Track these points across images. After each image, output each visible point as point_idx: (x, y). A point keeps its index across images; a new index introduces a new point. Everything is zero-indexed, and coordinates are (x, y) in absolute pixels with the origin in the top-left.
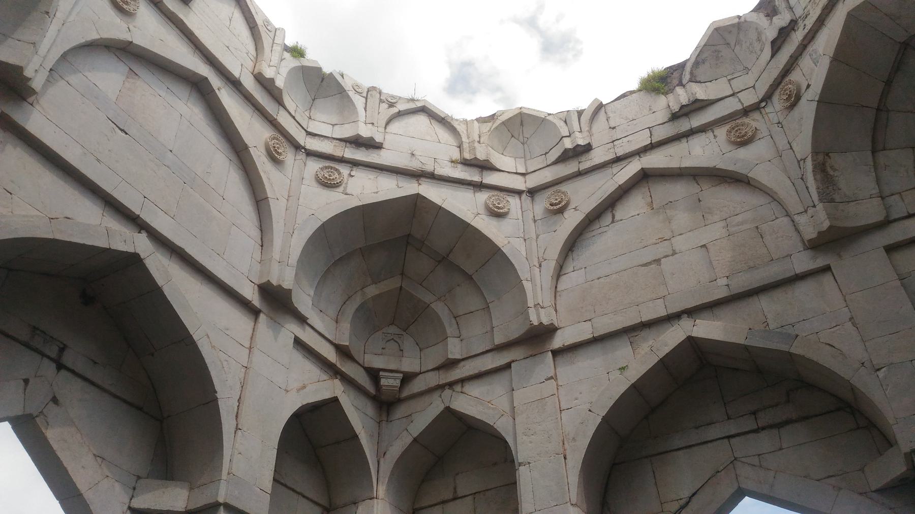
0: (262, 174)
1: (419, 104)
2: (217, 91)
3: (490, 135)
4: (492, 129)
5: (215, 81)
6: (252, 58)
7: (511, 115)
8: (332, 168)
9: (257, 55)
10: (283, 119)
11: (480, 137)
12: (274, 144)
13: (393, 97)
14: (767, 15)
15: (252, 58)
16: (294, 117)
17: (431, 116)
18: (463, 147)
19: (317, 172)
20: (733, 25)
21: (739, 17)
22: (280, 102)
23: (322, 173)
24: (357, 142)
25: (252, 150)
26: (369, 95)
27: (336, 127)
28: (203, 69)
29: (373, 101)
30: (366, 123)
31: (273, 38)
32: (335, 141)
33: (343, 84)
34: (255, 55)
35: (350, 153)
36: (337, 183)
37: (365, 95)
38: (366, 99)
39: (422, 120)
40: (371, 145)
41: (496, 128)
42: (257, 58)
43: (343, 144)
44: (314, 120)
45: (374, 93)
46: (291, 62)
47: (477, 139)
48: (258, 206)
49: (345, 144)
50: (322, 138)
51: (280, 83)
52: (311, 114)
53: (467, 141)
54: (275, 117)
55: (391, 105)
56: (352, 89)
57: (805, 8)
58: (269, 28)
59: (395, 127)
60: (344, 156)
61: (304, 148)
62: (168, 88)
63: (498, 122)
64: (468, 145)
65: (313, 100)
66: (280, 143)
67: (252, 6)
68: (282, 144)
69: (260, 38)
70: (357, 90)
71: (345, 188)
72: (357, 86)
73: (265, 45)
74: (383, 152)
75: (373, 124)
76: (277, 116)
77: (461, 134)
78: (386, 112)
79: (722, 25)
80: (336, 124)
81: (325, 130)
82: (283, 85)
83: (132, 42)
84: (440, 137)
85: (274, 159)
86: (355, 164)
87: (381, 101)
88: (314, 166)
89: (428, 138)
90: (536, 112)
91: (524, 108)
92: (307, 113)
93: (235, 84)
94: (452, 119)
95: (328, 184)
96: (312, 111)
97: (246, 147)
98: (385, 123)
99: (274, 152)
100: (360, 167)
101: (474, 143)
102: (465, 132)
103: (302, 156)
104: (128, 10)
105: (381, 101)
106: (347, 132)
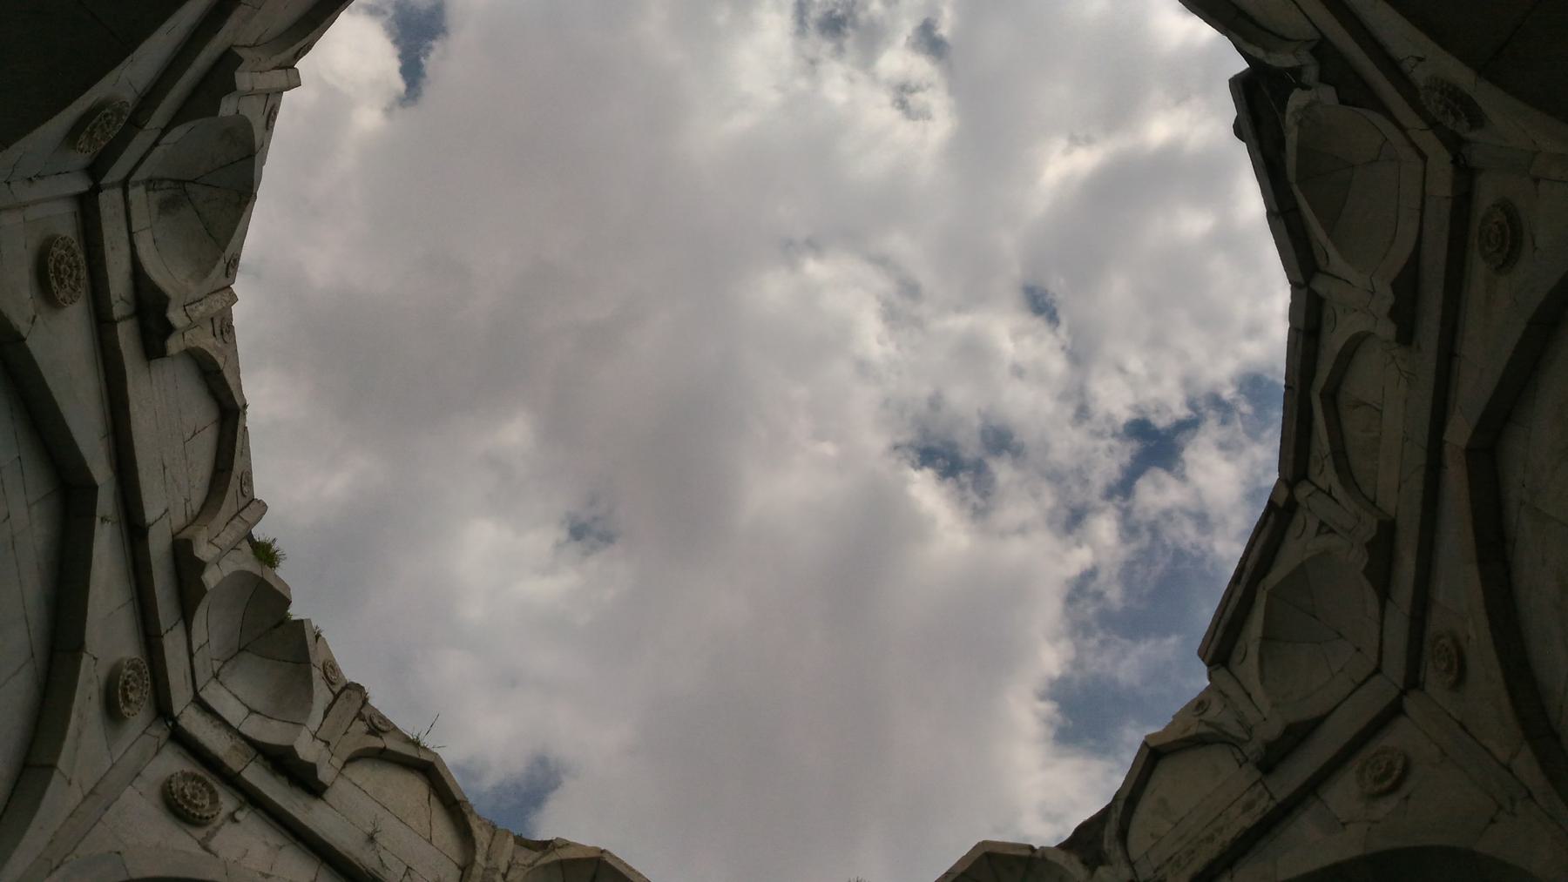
0: (74, 716)
1: (424, 756)
2: (98, 520)
3: (528, 874)
4: (539, 863)
5: (106, 502)
6: (189, 513)
7: (581, 855)
8: (205, 783)
9: (199, 513)
10: (173, 646)
11: (509, 868)
12: (129, 676)
13: (383, 719)
14: (1084, 862)
15: (189, 513)
16: (191, 655)
17: (435, 788)
18: (471, 870)
19: (172, 776)
20: (1018, 858)
21: (1031, 848)
22: (186, 614)
23: (182, 784)
24: (282, 762)
25: (86, 660)
26: (343, 695)
27: (254, 717)
28: (101, 471)
29: (347, 707)
30: (314, 737)
31: (241, 506)
32: (238, 739)
33: (311, 649)
34: (196, 513)
35: (256, 776)
36: (200, 817)
37: (337, 689)
38: (336, 697)
39: (414, 789)
40: (306, 780)
41: (546, 866)
42: (196, 518)
43: (252, 752)
44: (221, 683)
45: (355, 695)
46: (244, 561)
47: (503, 869)
48: (12, 794)
49: (254, 754)
50: (218, 722)
51: (211, 578)
52: (223, 671)
53: (484, 864)
54: (163, 631)
55: (374, 731)
56: (321, 667)
57: (1158, 868)
58: (245, 489)
59: (364, 774)
60: (242, 773)
61: (175, 720)
62: (19, 457)
63: (553, 857)
64: (481, 872)
65: (240, 650)
66: (140, 681)
67: (241, 437)
68: (142, 685)
69: (224, 493)
70: (329, 674)
71: (210, 836)
72: (332, 668)
73: (225, 507)
74: (318, 806)
75: (328, 744)
76: (167, 631)
77: (478, 846)
78: (358, 738)
79: (999, 850)
80: (258, 713)
81: (232, 711)
82: (213, 586)
83: (24, 340)
84: (435, 833)
85: (112, 710)
86: (254, 800)
87: (360, 716)
88: (172, 763)
89: (414, 823)
90: (628, 870)
91: (609, 853)
92: (217, 665)
93: (134, 529)
94: (472, 812)
95: (178, 808)
96: (227, 668)
97: (79, 647)
98: (353, 749)
99: (120, 692)
100: (259, 811)
101: (495, 874)
102: (486, 846)
103: (161, 732)
104: (55, 291)
105: (360, 716)
106: (271, 733)
